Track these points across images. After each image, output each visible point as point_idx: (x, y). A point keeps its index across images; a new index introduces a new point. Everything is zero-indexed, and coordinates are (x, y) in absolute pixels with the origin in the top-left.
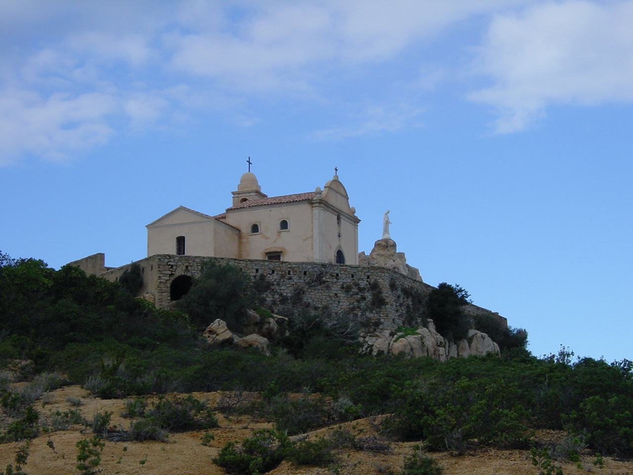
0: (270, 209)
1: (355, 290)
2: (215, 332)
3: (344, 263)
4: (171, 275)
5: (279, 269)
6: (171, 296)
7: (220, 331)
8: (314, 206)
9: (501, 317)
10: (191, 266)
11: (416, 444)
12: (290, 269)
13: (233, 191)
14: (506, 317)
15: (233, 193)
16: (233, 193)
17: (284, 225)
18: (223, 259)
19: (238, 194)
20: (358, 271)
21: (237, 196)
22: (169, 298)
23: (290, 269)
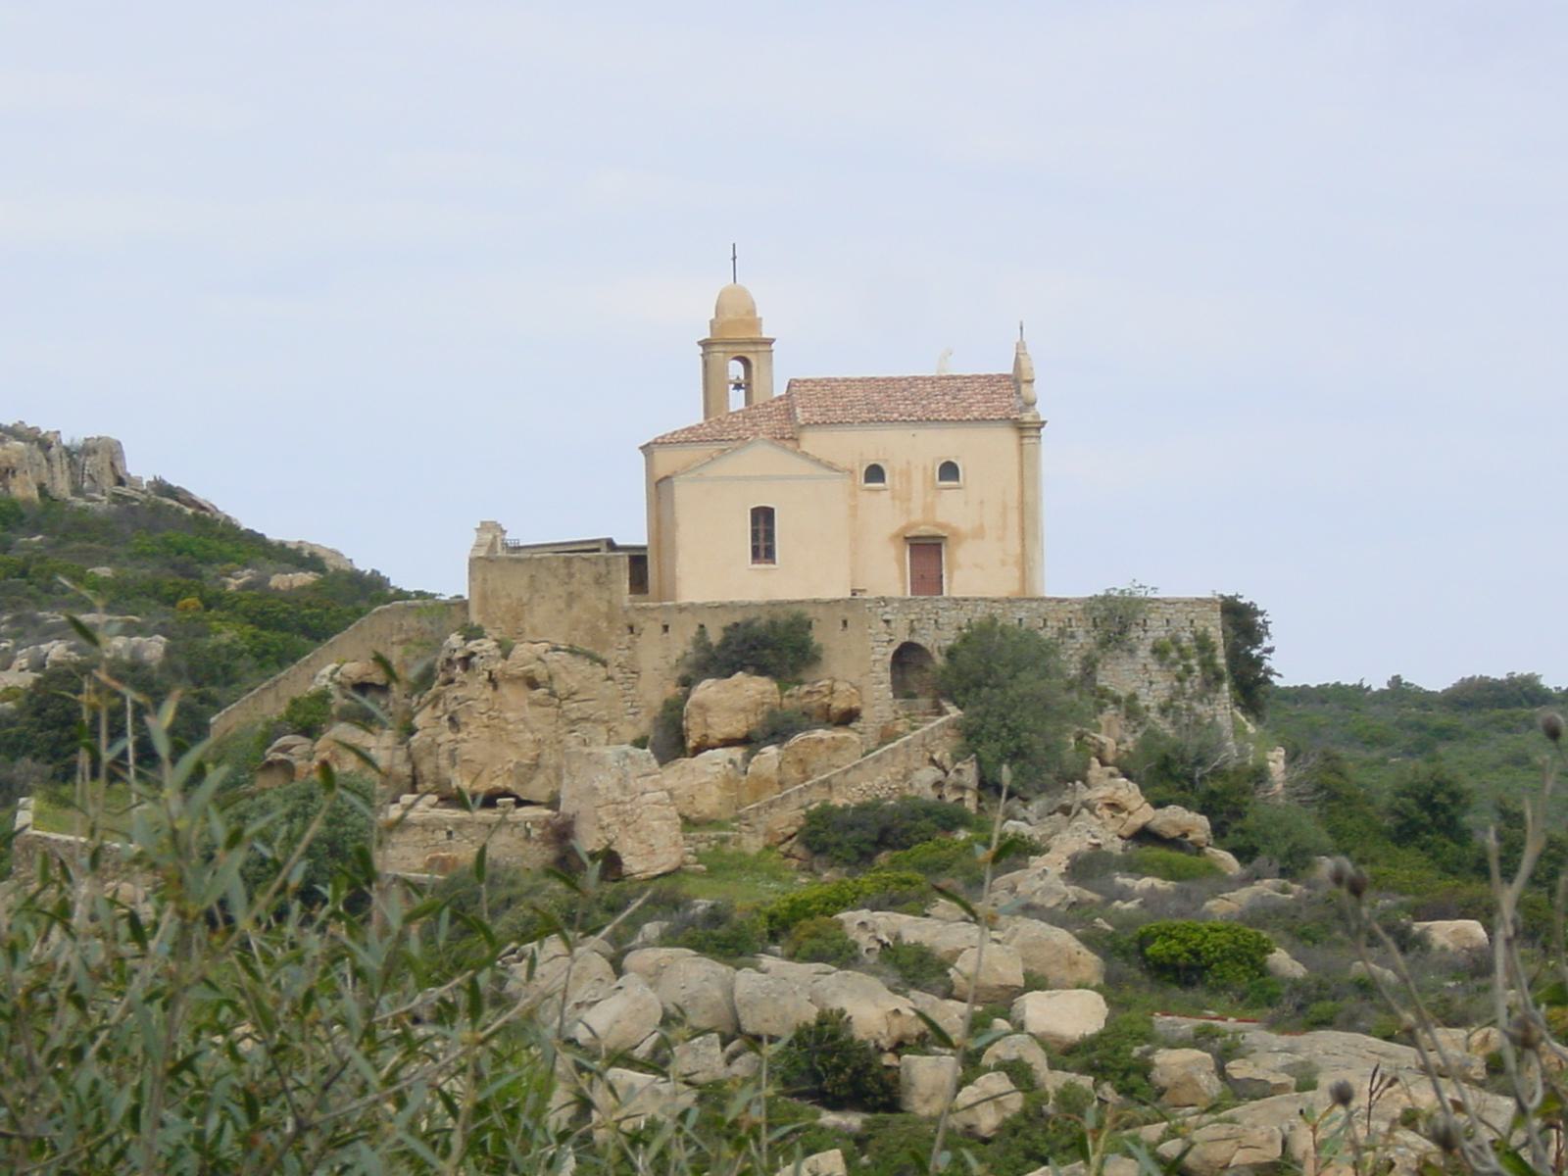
0: (913, 432)
1: (1174, 655)
3: (673, 597)
5: (1053, 615)
6: (893, 690)
8: (1027, 434)
9: (1062, 927)
12: (1070, 615)
13: (700, 339)
18: (966, 600)
20: (1177, 612)
22: (891, 695)
23: (1070, 615)
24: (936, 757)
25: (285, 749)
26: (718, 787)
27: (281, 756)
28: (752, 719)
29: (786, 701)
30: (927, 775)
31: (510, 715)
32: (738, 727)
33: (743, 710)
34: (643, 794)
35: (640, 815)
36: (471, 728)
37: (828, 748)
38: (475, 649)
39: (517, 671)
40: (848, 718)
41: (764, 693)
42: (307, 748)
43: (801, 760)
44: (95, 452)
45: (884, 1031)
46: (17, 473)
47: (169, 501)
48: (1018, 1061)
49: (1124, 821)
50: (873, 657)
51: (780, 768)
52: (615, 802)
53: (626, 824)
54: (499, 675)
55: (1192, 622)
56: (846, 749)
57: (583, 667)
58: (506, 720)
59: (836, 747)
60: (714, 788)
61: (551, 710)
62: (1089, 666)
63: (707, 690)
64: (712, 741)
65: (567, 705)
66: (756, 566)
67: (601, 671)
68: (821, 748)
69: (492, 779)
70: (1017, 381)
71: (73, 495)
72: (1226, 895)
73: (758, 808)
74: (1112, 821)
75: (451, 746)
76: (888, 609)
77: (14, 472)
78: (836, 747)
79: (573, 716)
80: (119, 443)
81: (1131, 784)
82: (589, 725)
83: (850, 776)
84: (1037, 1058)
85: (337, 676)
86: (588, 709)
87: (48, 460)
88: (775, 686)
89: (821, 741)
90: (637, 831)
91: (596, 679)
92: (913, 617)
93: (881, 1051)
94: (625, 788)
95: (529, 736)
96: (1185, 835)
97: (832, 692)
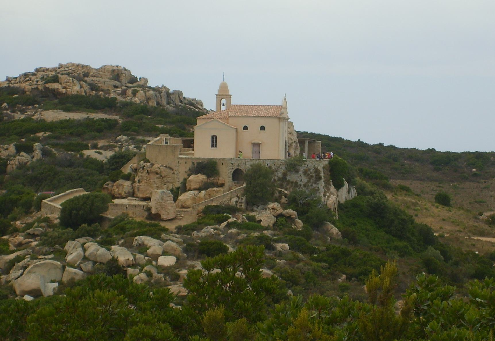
2: (276, 210)
4: (232, 168)
7: (278, 209)
8: (281, 120)
10: (241, 164)
11: (143, 138)
12: (281, 163)
14: (306, 131)
15: (216, 95)
16: (216, 95)
17: (262, 128)
19: (219, 95)
21: (218, 96)
24: (238, 195)
25: (108, 185)
26: (191, 200)
27: (106, 186)
28: (201, 185)
29: (208, 181)
30: (235, 199)
31: (151, 180)
32: (197, 186)
33: (199, 182)
34: (167, 201)
35: (166, 206)
36: (143, 183)
37: (216, 192)
38: (146, 165)
39: (154, 170)
40: (222, 185)
41: (203, 179)
42: (112, 184)
43: (209, 194)
44: (174, 94)
45: (125, 263)
46: (151, 99)
47: (192, 107)
48: (150, 271)
49: (275, 212)
50: (228, 172)
51: (205, 196)
52: (159, 202)
53: (162, 208)
54: (150, 171)
55: (314, 165)
56: (220, 192)
57: (168, 170)
58: (150, 181)
59: (217, 192)
60: (190, 200)
61: (160, 180)
62: (285, 175)
63: (192, 177)
64: (191, 189)
65: (165, 179)
66: (213, 149)
67: (172, 172)
68: (214, 192)
69: (146, 194)
70: (282, 108)
71: (167, 104)
72: (241, 235)
73: (196, 205)
74: (272, 212)
75: (138, 187)
76: (233, 161)
77: (150, 99)
78: (217, 192)
79: (165, 181)
80: (181, 92)
81: (278, 204)
82: (169, 183)
83: (217, 199)
84: (154, 271)
85: (132, 167)
86: (169, 180)
87: (160, 96)
88: (206, 177)
89: (214, 190)
90: (165, 209)
91: (171, 173)
92: (239, 163)
93: (124, 267)
94: (163, 199)
95: (155, 185)
96: (291, 216)
97: (218, 179)
